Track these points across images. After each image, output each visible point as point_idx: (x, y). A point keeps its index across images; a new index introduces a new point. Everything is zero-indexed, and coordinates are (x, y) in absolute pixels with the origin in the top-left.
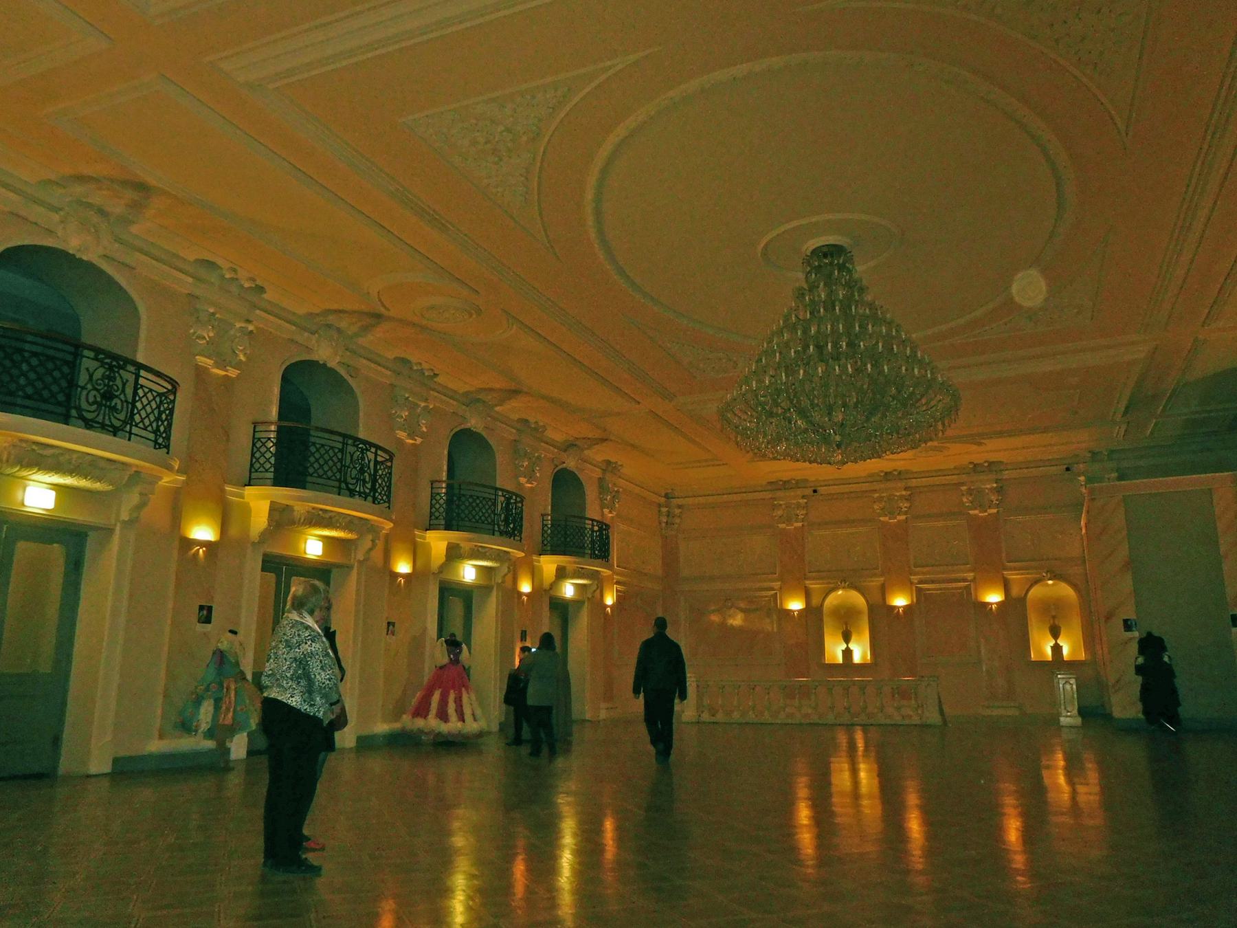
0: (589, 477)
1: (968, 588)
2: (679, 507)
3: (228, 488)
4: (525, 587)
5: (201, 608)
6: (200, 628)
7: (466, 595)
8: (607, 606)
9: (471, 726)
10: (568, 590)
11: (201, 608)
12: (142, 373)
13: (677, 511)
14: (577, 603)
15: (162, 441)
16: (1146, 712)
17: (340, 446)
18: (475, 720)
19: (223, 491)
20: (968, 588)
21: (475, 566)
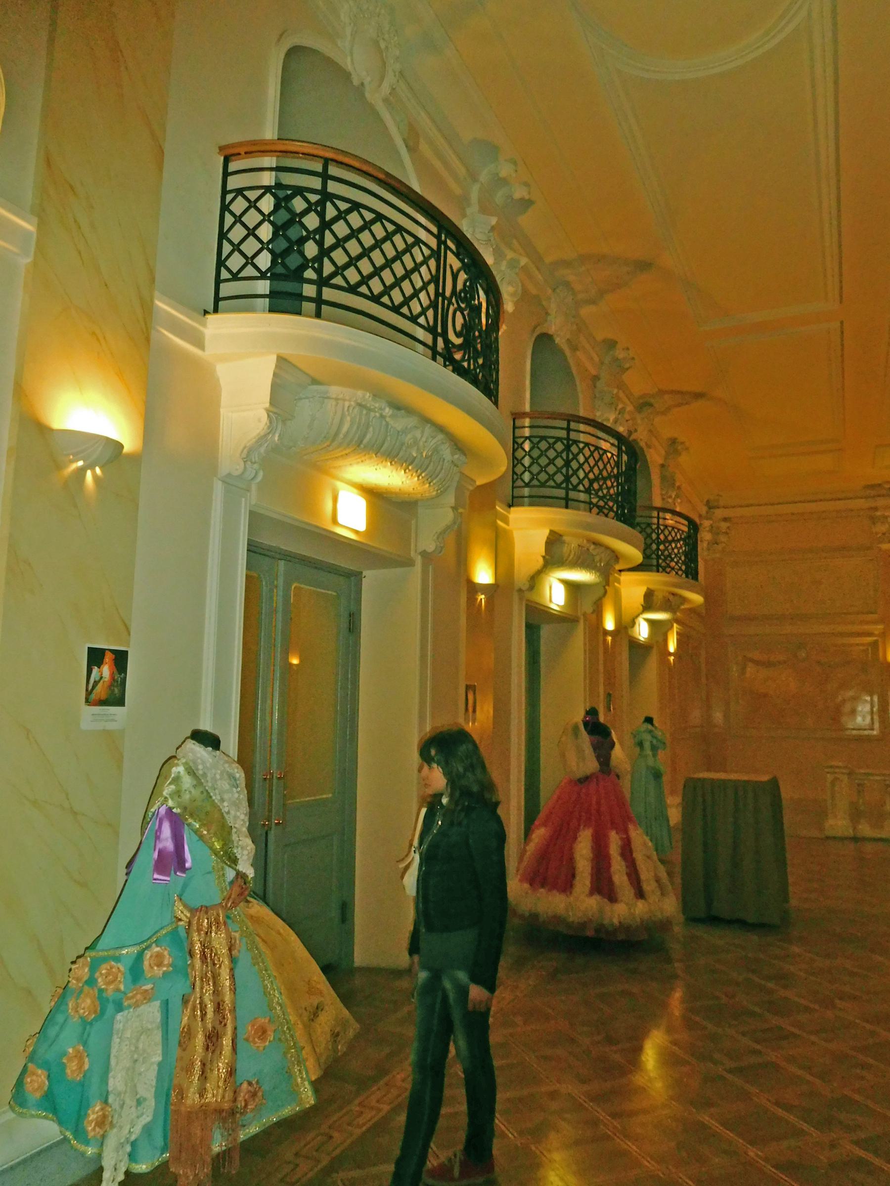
0: (654, 457)
1: (875, 645)
2: (725, 520)
3: (160, 304)
4: (483, 573)
5: (95, 657)
6: (91, 717)
7: (336, 570)
8: (606, 633)
9: (625, 910)
10: (555, 594)
11: (95, 657)
12: (573, 425)
13: (724, 525)
14: (565, 620)
15: (692, 573)
16: (218, 1154)
17: (563, 434)
18: (640, 894)
19: (148, 308)
20: (875, 645)
21: (647, 620)
